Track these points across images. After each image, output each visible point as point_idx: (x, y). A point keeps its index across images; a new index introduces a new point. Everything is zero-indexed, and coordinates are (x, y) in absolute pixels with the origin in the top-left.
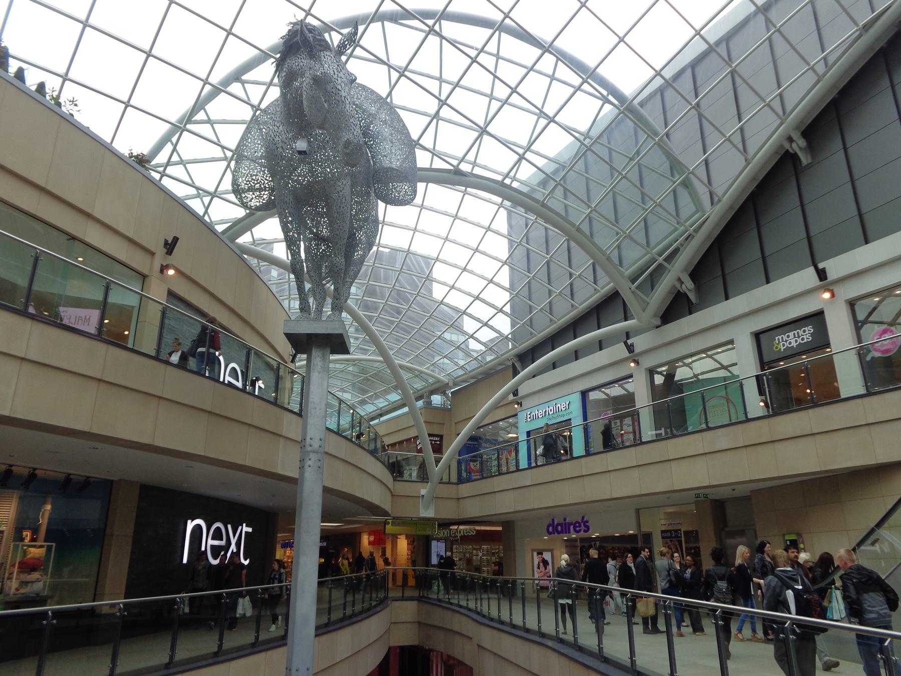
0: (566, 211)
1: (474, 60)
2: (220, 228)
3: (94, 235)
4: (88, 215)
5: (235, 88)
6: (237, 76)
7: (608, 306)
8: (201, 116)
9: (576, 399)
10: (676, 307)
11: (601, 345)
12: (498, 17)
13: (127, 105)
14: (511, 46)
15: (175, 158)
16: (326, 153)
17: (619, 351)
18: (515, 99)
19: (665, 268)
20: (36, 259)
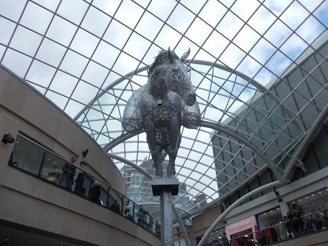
0: (109, 189)
1: (205, 77)
2: (102, 147)
3: (57, 149)
4: (55, 140)
5: (111, 91)
6: (111, 87)
7: (267, 174)
8: (96, 103)
9: (253, 218)
10: (297, 174)
11: (262, 193)
12: (213, 60)
13: (183, 36)
14: (217, 71)
15: (85, 120)
16: (164, 105)
17: (272, 195)
18: (222, 92)
19: (290, 157)
20: (45, 154)
